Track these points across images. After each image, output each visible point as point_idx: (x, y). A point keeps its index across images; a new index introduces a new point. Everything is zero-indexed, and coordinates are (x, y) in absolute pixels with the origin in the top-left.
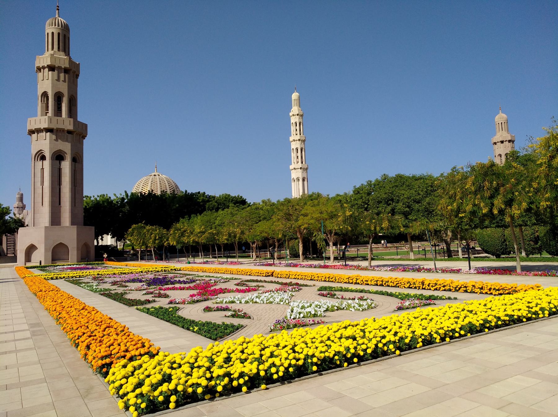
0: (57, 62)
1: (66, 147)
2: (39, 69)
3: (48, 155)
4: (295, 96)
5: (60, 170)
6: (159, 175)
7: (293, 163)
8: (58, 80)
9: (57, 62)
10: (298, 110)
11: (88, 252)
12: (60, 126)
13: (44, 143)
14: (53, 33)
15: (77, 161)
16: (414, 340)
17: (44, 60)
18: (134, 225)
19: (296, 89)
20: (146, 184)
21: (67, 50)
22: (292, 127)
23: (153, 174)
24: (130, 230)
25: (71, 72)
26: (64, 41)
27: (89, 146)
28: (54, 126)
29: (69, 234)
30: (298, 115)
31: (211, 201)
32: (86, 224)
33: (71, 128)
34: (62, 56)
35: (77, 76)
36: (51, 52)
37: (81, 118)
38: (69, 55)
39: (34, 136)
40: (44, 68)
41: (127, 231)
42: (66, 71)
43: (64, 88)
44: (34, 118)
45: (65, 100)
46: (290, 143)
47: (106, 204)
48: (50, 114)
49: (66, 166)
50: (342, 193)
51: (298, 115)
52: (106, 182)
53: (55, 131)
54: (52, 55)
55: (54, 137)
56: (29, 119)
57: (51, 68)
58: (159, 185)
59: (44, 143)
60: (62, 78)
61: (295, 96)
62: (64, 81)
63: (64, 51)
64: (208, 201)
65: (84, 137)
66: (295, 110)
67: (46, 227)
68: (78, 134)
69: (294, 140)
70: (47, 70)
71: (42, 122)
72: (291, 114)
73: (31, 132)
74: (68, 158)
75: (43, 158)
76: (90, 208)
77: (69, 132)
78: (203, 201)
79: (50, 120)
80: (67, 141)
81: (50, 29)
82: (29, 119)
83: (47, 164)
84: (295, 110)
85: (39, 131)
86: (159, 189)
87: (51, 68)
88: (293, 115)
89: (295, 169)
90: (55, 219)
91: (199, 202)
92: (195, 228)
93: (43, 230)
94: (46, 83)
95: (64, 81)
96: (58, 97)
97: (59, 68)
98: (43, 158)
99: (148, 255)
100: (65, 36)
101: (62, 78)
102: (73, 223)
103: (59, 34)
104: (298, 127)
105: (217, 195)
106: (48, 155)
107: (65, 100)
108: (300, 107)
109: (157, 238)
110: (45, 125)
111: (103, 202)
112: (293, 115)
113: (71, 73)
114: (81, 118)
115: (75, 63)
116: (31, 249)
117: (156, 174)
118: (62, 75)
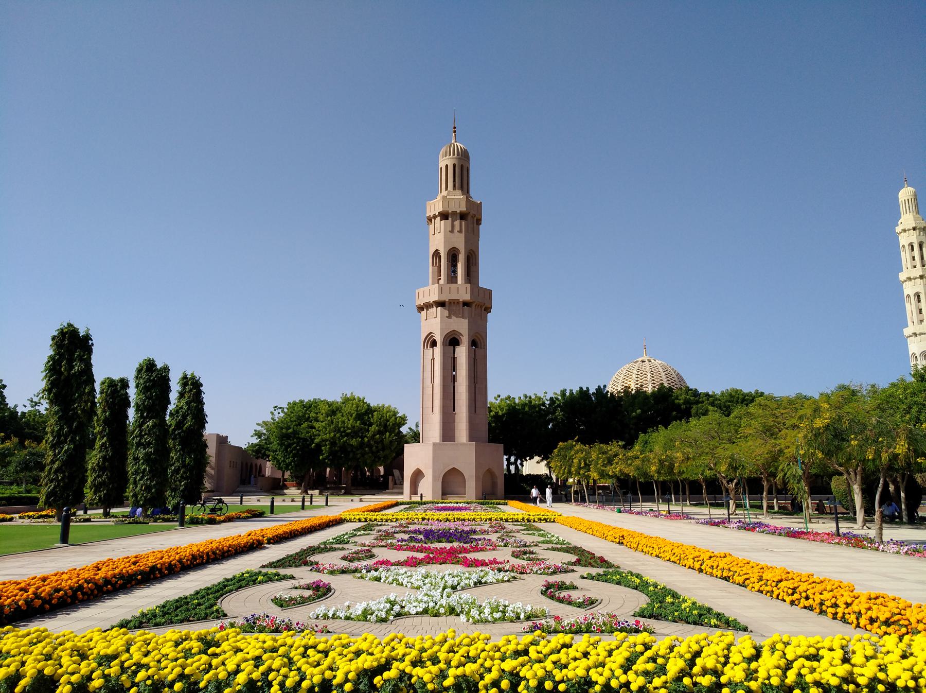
0: (451, 204)
1: (462, 326)
2: (430, 219)
3: (438, 339)
4: (905, 194)
5: (454, 359)
6: (649, 361)
7: (910, 323)
8: (452, 231)
9: (451, 204)
10: (915, 219)
11: (494, 484)
12: (454, 297)
13: (434, 323)
14: (447, 166)
15: (478, 344)
16: (202, 520)
17: (435, 207)
18: (561, 443)
19: (906, 181)
20: (628, 375)
21: (465, 186)
22: (903, 254)
23: (640, 359)
24: (556, 451)
25: (469, 217)
26: (461, 175)
27: (494, 323)
28: (446, 297)
29: (465, 456)
30: (914, 229)
31: (703, 402)
32: (491, 441)
33: (467, 297)
34: (459, 196)
35: (479, 222)
36: (444, 193)
37: (484, 282)
38: (468, 192)
39: (424, 313)
40: (435, 217)
41: (551, 452)
42: (463, 216)
43: (459, 242)
44: (422, 289)
45: (463, 260)
46: (899, 286)
47: (527, 409)
48: (442, 282)
49: (462, 353)
50: (46, 360)
51: (914, 229)
52: (522, 375)
53: (447, 304)
54: (444, 197)
55: (446, 313)
56: (417, 291)
57: (444, 216)
58: (649, 377)
59: (434, 323)
60: (457, 228)
61: (905, 194)
62: (460, 231)
63: (462, 188)
64: (697, 402)
65: (488, 309)
66: (908, 219)
67: (434, 444)
68: (478, 307)
69: (909, 279)
70: (438, 218)
71: (430, 293)
72: (898, 229)
73: (420, 309)
74: (465, 341)
75: (434, 344)
76: (503, 415)
77: (466, 304)
78: (687, 402)
79: (441, 290)
80: (463, 317)
81: (445, 161)
82: (417, 291)
83: (438, 350)
84: (908, 219)
85: (427, 306)
86: (650, 384)
87: (444, 216)
88: (905, 231)
89: (915, 334)
90: (448, 434)
91: (679, 405)
92: (658, 449)
93: (431, 448)
94: (438, 238)
95: (460, 231)
96: (453, 256)
97: (454, 213)
98: (434, 344)
99: (599, 494)
100: (462, 167)
101: (457, 228)
102: (471, 438)
103: (454, 166)
104: (916, 253)
105: (718, 392)
106: (438, 339)
107: (463, 260)
108: (918, 212)
109: (582, 465)
110: (434, 298)
111: (524, 405)
112: (905, 231)
113: (469, 218)
114: (483, 283)
115: (475, 203)
116: (418, 475)
117: (645, 358)
118: (457, 223)
